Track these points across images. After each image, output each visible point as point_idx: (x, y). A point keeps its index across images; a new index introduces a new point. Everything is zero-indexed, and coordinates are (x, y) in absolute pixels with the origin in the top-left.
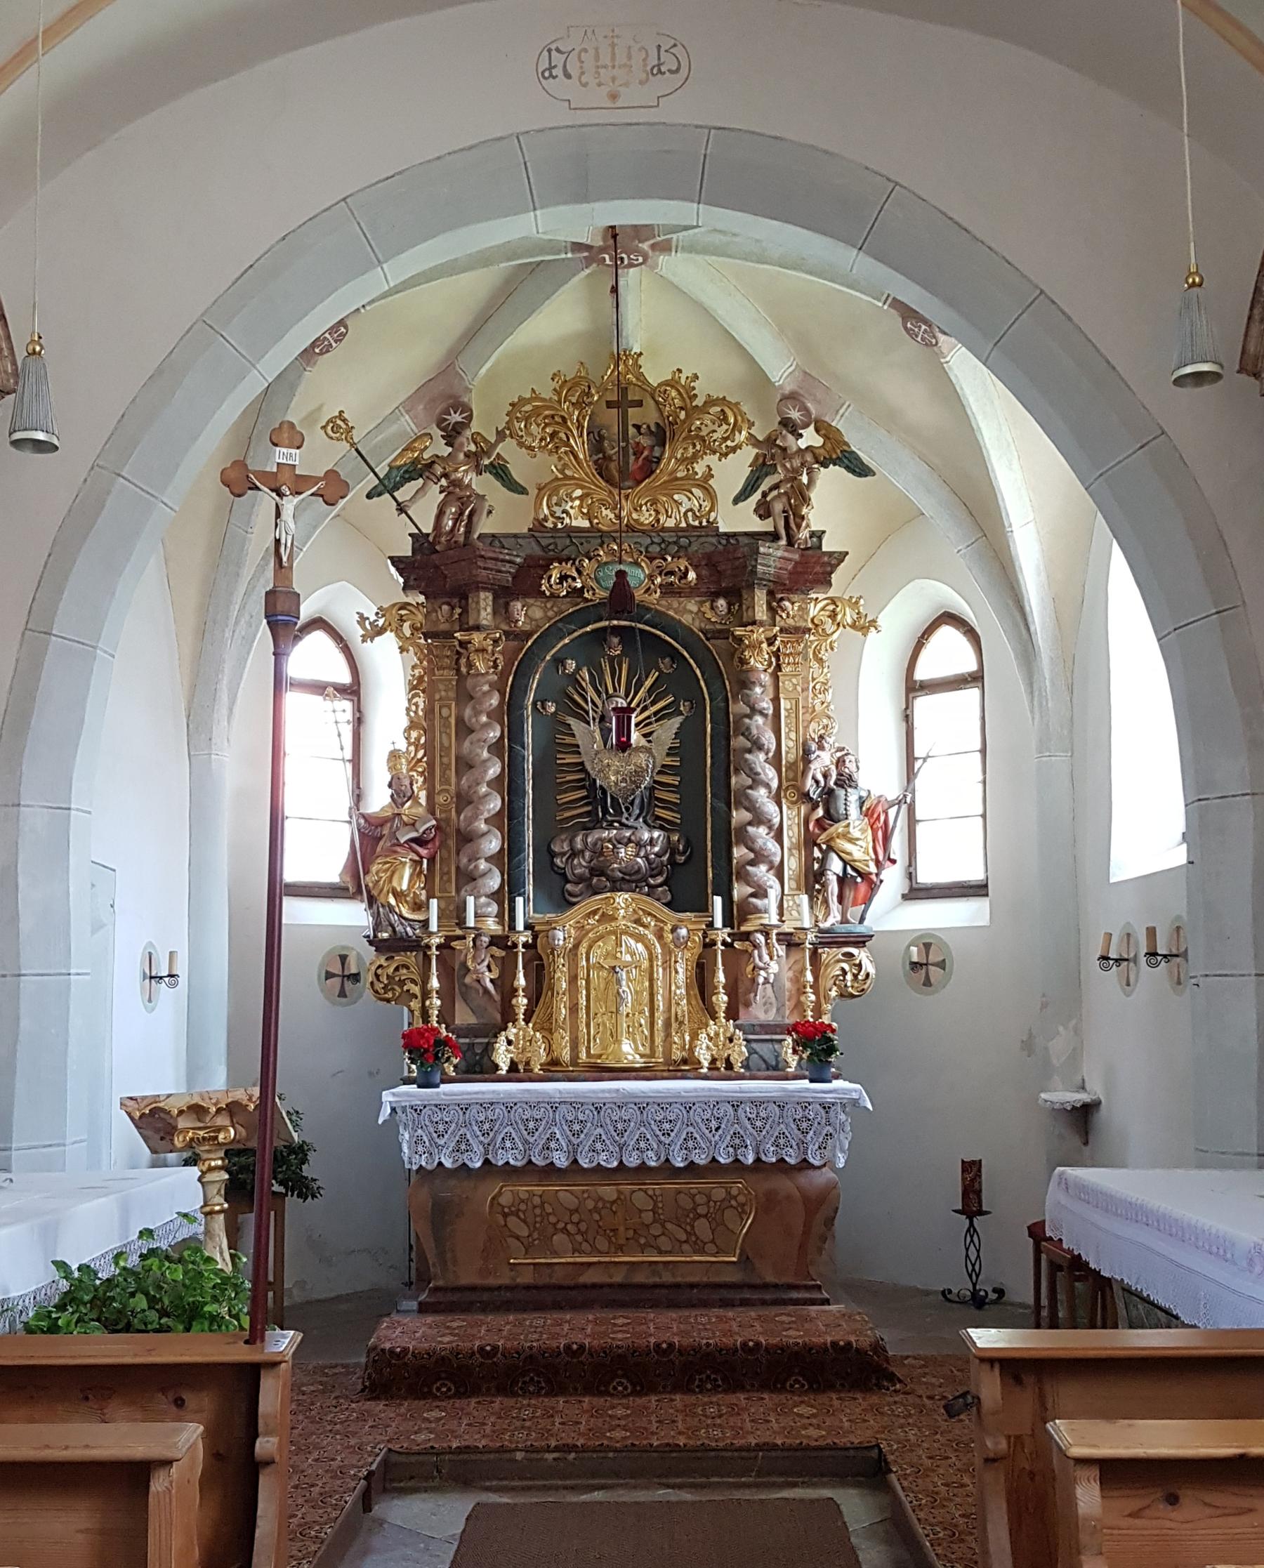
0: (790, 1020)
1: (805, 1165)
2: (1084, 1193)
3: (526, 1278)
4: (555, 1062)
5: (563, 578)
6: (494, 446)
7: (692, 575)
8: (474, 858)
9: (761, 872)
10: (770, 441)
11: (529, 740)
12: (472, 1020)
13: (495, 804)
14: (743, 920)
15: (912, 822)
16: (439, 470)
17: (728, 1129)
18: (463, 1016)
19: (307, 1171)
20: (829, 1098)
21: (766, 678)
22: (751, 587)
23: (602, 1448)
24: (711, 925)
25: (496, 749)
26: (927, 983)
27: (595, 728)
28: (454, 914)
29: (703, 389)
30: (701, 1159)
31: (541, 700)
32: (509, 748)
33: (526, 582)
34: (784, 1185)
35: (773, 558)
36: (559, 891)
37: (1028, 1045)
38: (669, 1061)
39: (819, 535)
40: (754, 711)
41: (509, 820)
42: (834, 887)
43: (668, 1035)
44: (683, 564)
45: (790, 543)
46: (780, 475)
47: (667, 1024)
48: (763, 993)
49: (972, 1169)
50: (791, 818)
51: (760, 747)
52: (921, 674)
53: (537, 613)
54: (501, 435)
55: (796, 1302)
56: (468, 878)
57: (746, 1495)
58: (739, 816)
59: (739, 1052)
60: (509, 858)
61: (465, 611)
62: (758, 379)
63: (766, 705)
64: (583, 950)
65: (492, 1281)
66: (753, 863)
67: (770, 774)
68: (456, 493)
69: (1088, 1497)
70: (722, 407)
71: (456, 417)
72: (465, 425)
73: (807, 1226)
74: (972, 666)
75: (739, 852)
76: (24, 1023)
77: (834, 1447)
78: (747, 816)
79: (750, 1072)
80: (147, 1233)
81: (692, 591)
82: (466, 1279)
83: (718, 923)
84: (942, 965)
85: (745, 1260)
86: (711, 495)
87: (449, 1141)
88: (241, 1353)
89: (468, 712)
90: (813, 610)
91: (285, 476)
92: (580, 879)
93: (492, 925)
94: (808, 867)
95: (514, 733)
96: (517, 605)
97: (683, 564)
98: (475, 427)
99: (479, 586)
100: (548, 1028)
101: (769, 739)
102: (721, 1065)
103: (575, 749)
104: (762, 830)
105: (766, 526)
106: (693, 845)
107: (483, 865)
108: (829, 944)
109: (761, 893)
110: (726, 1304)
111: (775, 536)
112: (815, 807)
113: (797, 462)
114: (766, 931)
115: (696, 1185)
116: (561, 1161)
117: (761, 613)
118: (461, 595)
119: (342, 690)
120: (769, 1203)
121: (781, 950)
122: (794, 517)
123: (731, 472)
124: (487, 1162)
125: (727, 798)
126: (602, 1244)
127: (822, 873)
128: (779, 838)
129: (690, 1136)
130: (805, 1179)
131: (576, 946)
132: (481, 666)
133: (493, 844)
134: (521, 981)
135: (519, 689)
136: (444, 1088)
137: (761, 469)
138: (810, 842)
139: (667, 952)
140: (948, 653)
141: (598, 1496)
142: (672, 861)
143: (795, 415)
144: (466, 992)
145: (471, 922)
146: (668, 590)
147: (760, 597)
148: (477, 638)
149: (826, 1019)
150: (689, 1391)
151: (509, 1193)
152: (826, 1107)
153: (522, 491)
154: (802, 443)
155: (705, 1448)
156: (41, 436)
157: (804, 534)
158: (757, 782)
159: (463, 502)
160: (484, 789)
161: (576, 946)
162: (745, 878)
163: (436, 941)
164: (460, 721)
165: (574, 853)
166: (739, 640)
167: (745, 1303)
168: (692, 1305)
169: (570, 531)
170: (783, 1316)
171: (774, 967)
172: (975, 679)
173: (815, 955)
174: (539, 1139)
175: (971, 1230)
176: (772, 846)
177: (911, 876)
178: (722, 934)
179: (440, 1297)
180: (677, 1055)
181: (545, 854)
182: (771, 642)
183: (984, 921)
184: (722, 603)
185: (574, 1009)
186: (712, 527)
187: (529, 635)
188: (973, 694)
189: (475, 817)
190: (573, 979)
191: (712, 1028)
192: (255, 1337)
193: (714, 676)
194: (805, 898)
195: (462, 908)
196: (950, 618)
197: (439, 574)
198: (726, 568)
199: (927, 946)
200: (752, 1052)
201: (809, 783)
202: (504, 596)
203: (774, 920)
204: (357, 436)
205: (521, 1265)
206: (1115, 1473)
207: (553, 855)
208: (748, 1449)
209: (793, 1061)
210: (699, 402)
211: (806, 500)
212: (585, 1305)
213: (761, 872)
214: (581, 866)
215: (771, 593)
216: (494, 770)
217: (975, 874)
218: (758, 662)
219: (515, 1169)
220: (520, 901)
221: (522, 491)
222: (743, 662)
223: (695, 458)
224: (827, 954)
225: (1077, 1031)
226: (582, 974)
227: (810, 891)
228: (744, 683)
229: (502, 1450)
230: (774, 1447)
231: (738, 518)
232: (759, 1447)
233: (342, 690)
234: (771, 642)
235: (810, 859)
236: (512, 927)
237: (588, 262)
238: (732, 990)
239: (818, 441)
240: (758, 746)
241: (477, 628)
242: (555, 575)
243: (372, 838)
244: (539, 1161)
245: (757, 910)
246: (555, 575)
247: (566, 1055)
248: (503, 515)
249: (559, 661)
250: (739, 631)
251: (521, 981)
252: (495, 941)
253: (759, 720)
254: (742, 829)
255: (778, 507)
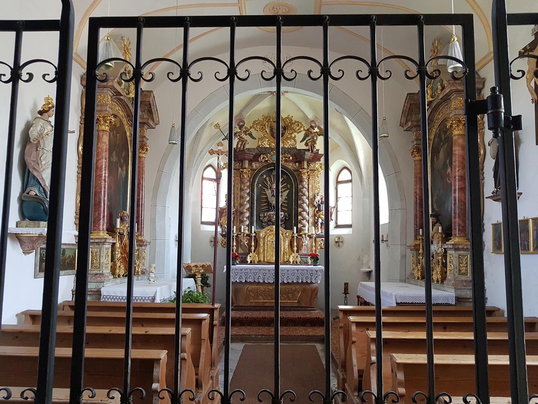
0: (310, 253)
1: (312, 283)
2: (365, 286)
3: (254, 304)
4: (259, 261)
5: (264, 158)
6: (249, 130)
7: (291, 158)
8: (243, 217)
9: (304, 222)
10: (308, 130)
11: (255, 192)
12: (243, 252)
13: (248, 206)
14: (300, 232)
15: (337, 211)
16: (238, 135)
17: (296, 275)
18: (241, 251)
19: (208, 282)
20: (317, 269)
21: (306, 180)
22: (304, 161)
23: (270, 335)
24: (293, 233)
25: (248, 194)
26: (339, 246)
27: (270, 191)
28: (239, 229)
29: (294, 119)
30: (290, 281)
31: (258, 184)
32: (251, 194)
33: (256, 158)
34: (307, 287)
35: (308, 155)
36: (261, 225)
37: (359, 259)
38: (284, 261)
39: (318, 150)
40: (304, 187)
41: (251, 209)
42: (320, 225)
43: (284, 256)
44: (289, 155)
45: (312, 152)
46: (310, 137)
47: (284, 254)
48: (304, 248)
49: (346, 285)
50: (311, 210)
51: (305, 195)
52: (339, 180)
53: (258, 165)
54: (251, 127)
55: (309, 310)
56: (242, 222)
57: (297, 344)
58: (300, 210)
59: (299, 260)
60: (251, 218)
61: (242, 164)
62: (306, 117)
63: (306, 186)
64: (266, 238)
65: (246, 305)
66: (303, 220)
67: (307, 201)
68: (241, 139)
69: (354, 328)
70: (298, 123)
71: (242, 124)
72: (243, 125)
73: (312, 295)
74: (350, 179)
75: (300, 217)
76: (157, 249)
77: (315, 336)
78: (302, 210)
79: (301, 264)
80: (189, 288)
81: (291, 161)
82: (241, 304)
83: (295, 232)
84: (342, 242)
85: (299, 302)
86: (295, 141)
87: (238, 276)
88: (211, 306)
89: (243, 186)
90: (317, 166)
91: (220, 152)
92: (266, 222)
93: (247, 232)
94: (314, 221)
95: (252, 191)
96: (253, 163)
97: (289, 155)
98: (245, 126)
99: (245, 159)
100: (258, 254)
101: (307, 193)
102: (295, 262)
103: (266, 194)
104: (305, 213)
105: (307, 148)
106: (290, 215)
107: (245, 219)
108: (318, 237)
109: (304, 226)
110: (294, 310)
111: (309, 150)
112: (316, 208)
113: (314, 135)
114: (305, 234)
115: (288, 287)
116: (261, 281)
117: (306, 166)
118: (242, 161)
119: (215, 180)
120: (304, 291)
121: (308, 238)
122: (313, 147)
123: (300, 136)
124: (246, 281)
125: (297, 206)
126: (269, 298)
127: (317, 222)
128: (308, 215)
129: (288, 277)
130: (311, 286)
131: (265, 237)
132: (246, 176)
133: (247, 214)
134: (253, 244)
135: (253, 182)
136: (237, 265)
137: (306, 136)
138: (315, 215)
139: (284, 238)
140: (345, 175)
141: (269, 344)
142: (285, 219)
143: (313, 125)
144: (241, 245)
145: (242, 231)
146: (286, 161)
147: (305, 163)
148: (245, 170)
149: (317, 253)
150: (286, 326)
151: (250, 287)
152: (316, 271)
153: (255, 139)
154: (315, 131)
155: (290, 336)
156: (174, 142)
157: (315, 150)
158: (304, 202)
159: (243, 141)
160: (246, 203)
161: (265, 237)
162: (301, 223)
163: (235, 235)
164: (241, 188)
165: (265, 217)
166: (301, 172)
167: (298, 310)
168: (287, 310)
169: (265, 148)
170: (306, 312)
171: (307, 242)
172: (350, 181)
173: (315, 240)
174: (257, 276)
175: (346, 297)
176: (307, 216)
177: (336, 223)
178: (296, 235)
179: (236, 308)
180: (286, 260)
181: (258, 217)
182: (308, 173)
183: (351, 233)
184: (297, 164)
185: (264, 250)
186: (295, 148)
187: (256, 170)
188: (350, 184)
189: (244, 209)
190: (264, 244)
191: (293, 255)
192: (213, 304)
193: (295, 179)
194: (313, 228)
195: (241, 228)
196: (345, 168)
197: (236, 158)
198: (298, 156)
199: (339, 238)
200: (301, 260)
201: (315, 203)
202: (251, 162)
203: (307, 232)
204: (221, 127)
205: (253, 302)
206: (358, 324)
207: (260, 217)
208: (298, 336)
209: (310, 262)
210: (293, 122)
211: (315, 143)
212: (266, 310)
213: (304, 222)
214: (266, 219)
215: (308, 162)
216: (248, 199)
217: (350, 223)
218: (305, 177)
219: (251, 283)
220: (253, 227)
221: (255, 139)
222: (302, 177)
223: (292, 133)
224: (318, 239)
225: (369, 256)
226: (266, 243)
227: (315, 226)
228: (302, 181)
229: (250, 335)
230: (304, 336)
231: (301, 146)
232: (300, 336)
233: (215, 180)
234: (308, 173)
235: (315, 219)
236: (251, 232)
237: (271, 94)
238: (297, 246)
239: (318, 131)
240: (304, 195)
241: (245, 168)
242: (262, 157)
243: (220, 212)
244: (257, 281)
245: (303, 230)
246: (262, 157)
247: (262, 260)
248: (251, 144)
249: (262, 175)
250: (301, 170)
251: (253, 244)
252: (248, 235)
253: (305, 189)
254: (300, 212)
255: (310, 144)
